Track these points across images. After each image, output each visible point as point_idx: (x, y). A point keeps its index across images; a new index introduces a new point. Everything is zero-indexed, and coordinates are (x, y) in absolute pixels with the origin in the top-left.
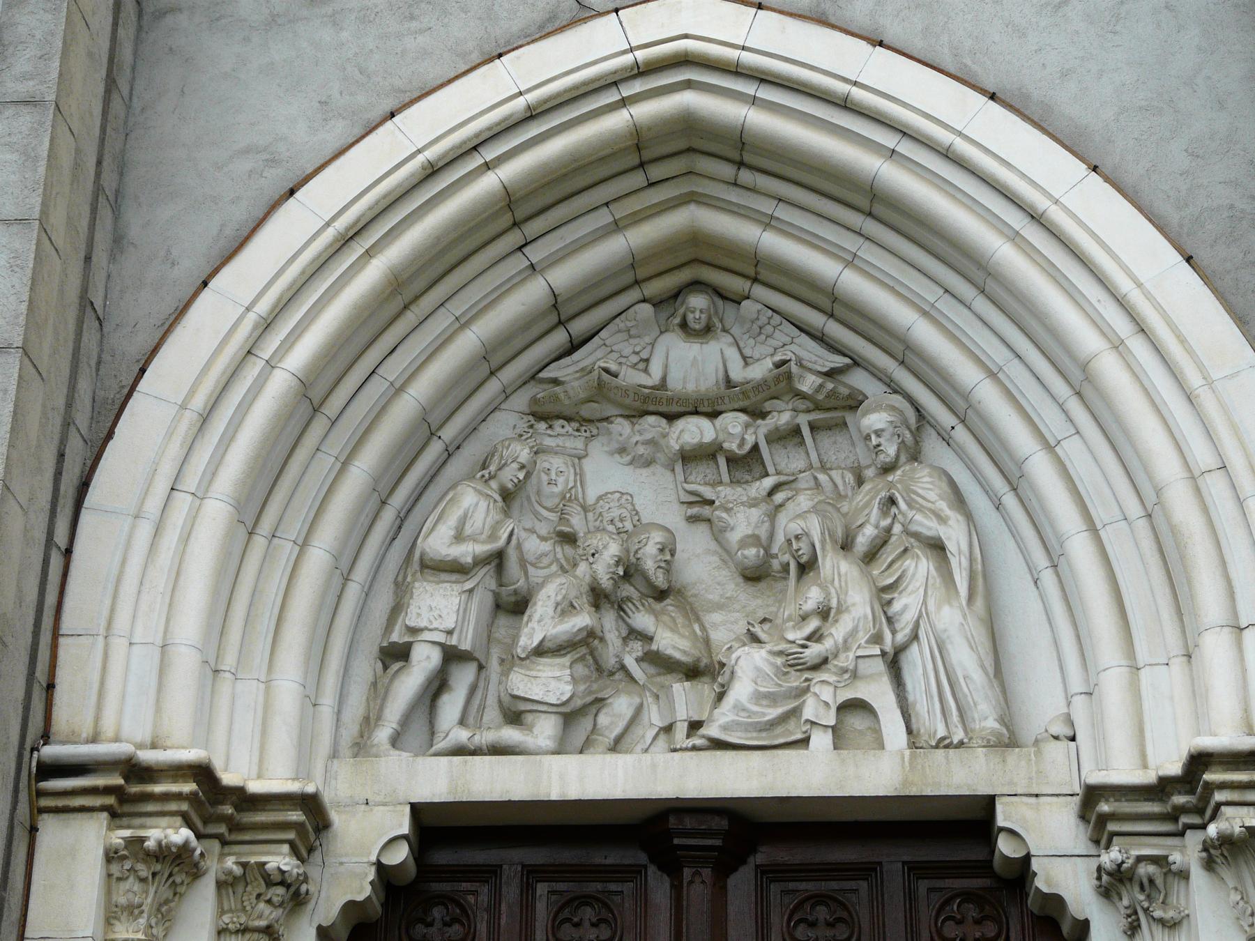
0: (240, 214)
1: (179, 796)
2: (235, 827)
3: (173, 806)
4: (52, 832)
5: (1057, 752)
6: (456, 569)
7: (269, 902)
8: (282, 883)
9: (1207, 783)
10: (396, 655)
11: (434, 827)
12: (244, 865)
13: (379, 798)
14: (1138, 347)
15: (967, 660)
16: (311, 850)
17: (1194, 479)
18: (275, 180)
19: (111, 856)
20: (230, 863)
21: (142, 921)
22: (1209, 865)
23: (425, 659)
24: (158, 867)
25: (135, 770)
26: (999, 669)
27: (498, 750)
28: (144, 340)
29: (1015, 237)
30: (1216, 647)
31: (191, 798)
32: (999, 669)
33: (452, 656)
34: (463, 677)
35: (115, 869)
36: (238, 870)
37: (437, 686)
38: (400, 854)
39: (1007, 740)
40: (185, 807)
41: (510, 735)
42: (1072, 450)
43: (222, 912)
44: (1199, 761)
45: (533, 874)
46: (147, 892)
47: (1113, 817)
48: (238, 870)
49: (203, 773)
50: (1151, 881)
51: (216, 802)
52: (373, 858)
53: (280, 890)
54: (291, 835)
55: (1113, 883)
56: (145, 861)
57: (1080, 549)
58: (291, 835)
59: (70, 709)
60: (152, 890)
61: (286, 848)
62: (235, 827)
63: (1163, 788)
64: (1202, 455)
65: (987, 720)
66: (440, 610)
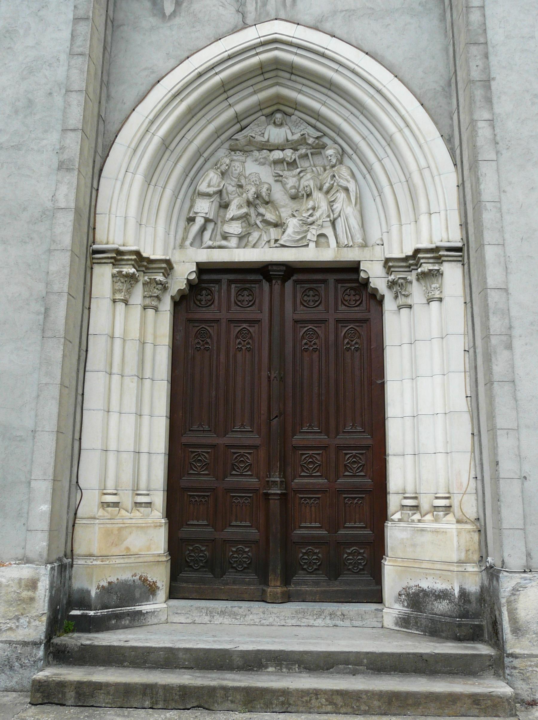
0: (143, 89)
1: (131, 260)
2: (147, 268)
3: (130, 262)
4: (97, 269)
5: (378, 249)
6: (208, 195)
7: (157, 289)
8: (161, 284)
9: (419, 258)
10: (191, 220)
11: (203, 269)
12: (150, 279)
13: (187, 261)
14: (406, 131)
15: (354, 223)
16: (168, 275)
17: (420, 170)
18: (153, 78)
19: (113, 276)
20: (146, 278)
21: (123, 294)
22: (418, 280)
23: (199, 221)
24: (126, 279)
25: (119, 253)
26: (363, 225)
27: (220, 247)
28: (116, 127)
29: (372, 97)
30: (424, 219)
31: (135, 260)
32: (363, 225)
33: (207, 220)
34: (210, 227)
35: (115, 279)
36: (148, 280)
37: (203, 229)
38: (193, 276)
39: (364, 245)
40: (133, 263)
41: (224, 243)
42: (386, 161)
43: (144, 292)
44: (417, 251)
45: (230, 282)
46: (124, 286)
47: (392, 267)
48: (148, 280)
49: (138, 253)
50: (402, 284)
51: (141, 261)
52: (186, 277)
53: (160, 286)
54: (163, 271)
55: (392, 285)
56: (123, 278)
57: (387, 190)
58: (163, 271)
59: (100, 235)
60: (125, 285)
61: (161, 274)
62: (147, 268)
63: (407, 258)
64: (423, 163)
65: (359, 239)
66: (204, 207)
